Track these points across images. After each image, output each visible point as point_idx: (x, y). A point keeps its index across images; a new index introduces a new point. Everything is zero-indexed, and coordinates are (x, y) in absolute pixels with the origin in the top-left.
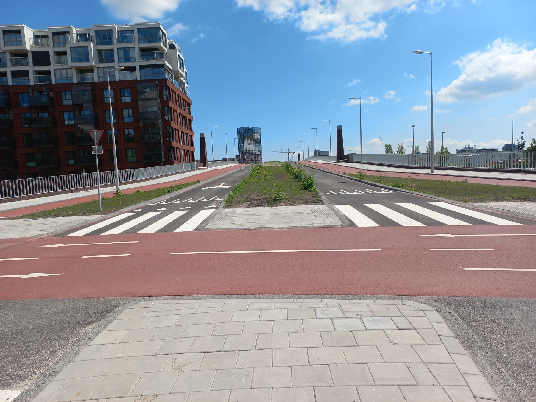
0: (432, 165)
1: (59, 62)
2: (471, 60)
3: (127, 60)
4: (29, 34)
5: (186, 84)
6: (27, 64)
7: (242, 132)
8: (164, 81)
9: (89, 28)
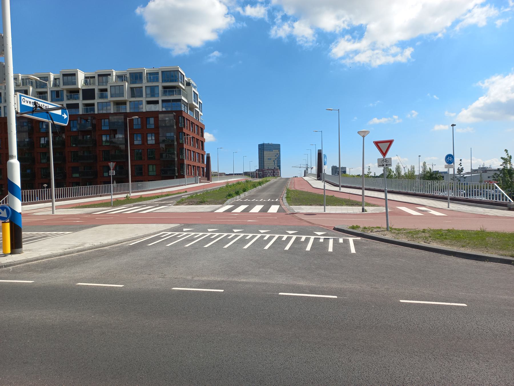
0: (363, 186)
1: (102, 97)
2: (493, 83)
3: (153, 95)
4: (81, 76)
5: (200, 113)
6: (78, 98)
7: (262, 148)
8: (179, 113)
9: (126, 70)
